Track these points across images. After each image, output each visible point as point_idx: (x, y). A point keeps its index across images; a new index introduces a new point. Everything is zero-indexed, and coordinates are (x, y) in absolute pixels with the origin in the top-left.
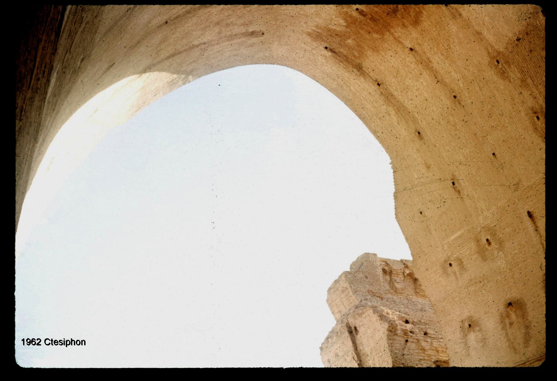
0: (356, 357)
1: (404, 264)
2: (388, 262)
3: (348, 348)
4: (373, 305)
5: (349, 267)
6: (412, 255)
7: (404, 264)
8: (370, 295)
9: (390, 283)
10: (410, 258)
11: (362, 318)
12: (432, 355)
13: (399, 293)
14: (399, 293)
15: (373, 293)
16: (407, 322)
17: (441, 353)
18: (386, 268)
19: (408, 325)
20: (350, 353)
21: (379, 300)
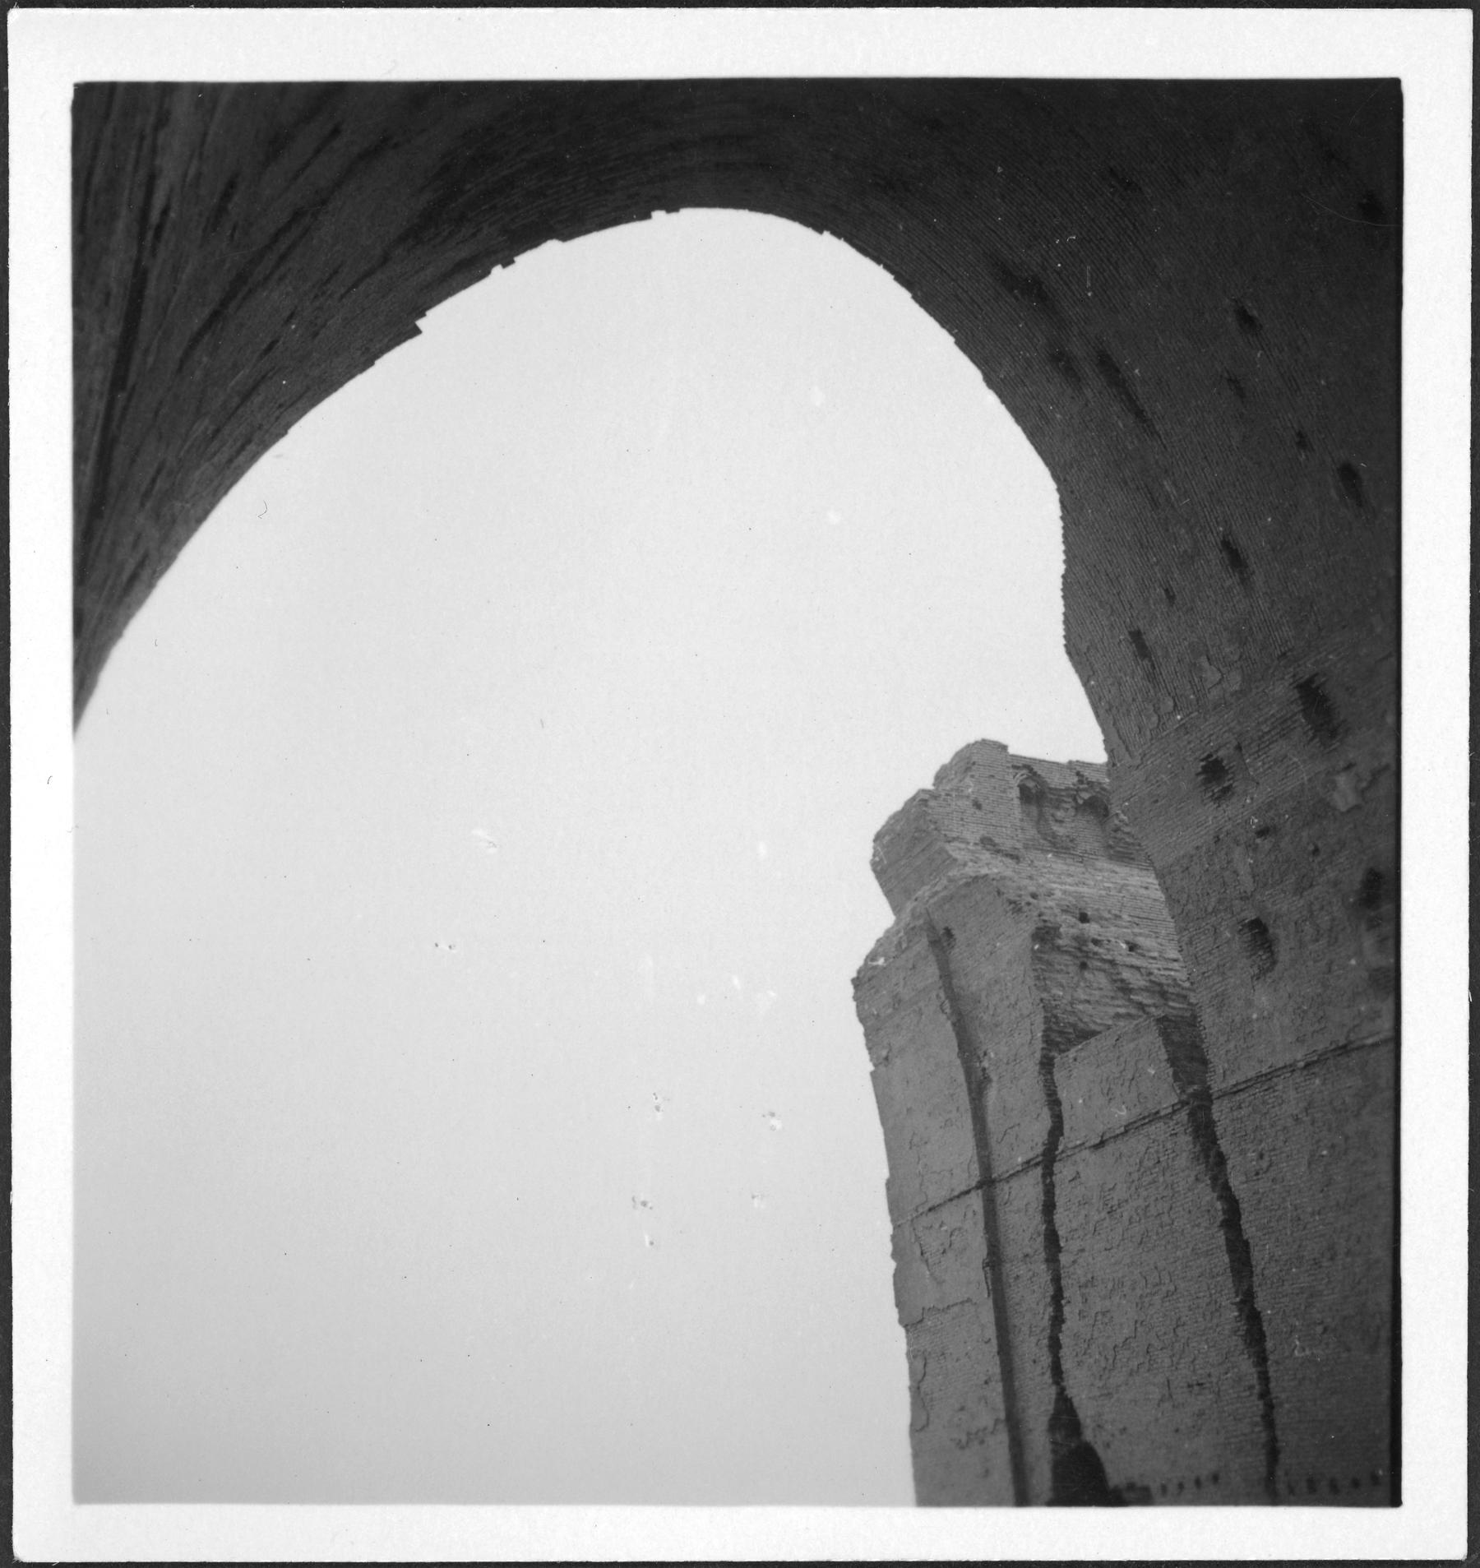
0: (947, 1005)
1: (1078, 774)
2: (1036, 769)
3: (1094, 491)
4: (991, 1381)
5: (932, 780)
6: (1110, 750)
7: (1078, 774)
8: (988, 850)
9: (1038, 822)
10: (1098, 755)
11: (940, 988)
12: (1149, 1006)
13: (1062, 847)
14: (1062, 847)
15: (994, 845)
16: (1084, 918)
17: (1173, 1000)
18: (1031, 784)
19: (1086, 925)
20: (933, 995)
21: (1010, 863)
